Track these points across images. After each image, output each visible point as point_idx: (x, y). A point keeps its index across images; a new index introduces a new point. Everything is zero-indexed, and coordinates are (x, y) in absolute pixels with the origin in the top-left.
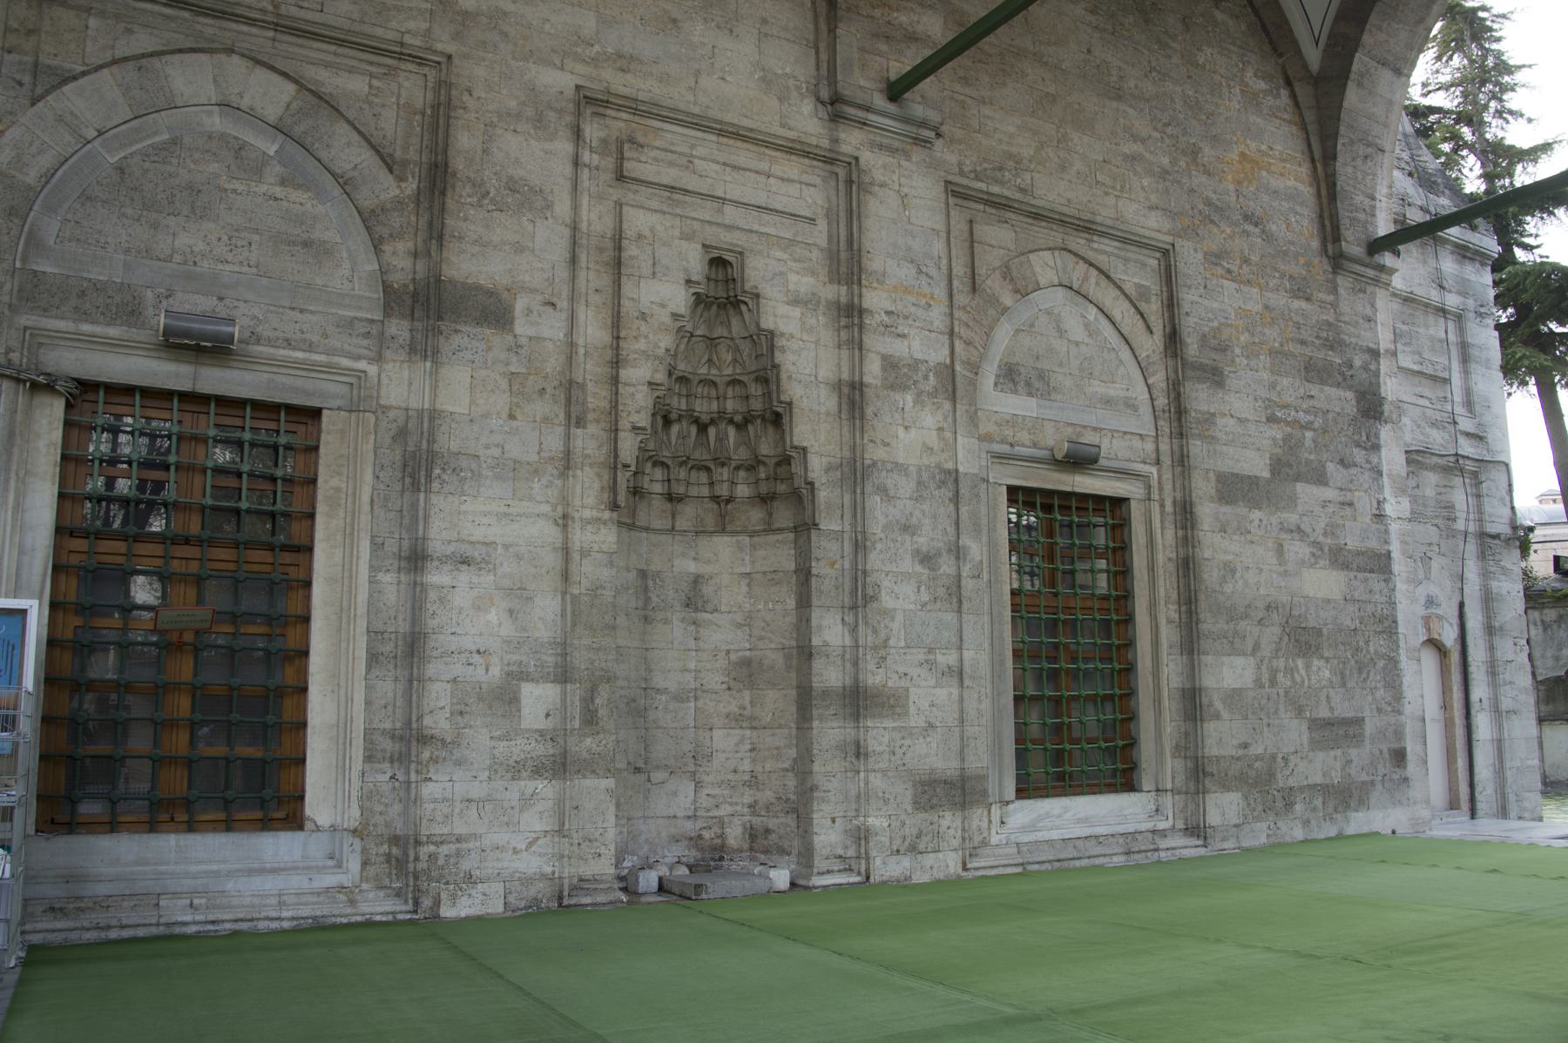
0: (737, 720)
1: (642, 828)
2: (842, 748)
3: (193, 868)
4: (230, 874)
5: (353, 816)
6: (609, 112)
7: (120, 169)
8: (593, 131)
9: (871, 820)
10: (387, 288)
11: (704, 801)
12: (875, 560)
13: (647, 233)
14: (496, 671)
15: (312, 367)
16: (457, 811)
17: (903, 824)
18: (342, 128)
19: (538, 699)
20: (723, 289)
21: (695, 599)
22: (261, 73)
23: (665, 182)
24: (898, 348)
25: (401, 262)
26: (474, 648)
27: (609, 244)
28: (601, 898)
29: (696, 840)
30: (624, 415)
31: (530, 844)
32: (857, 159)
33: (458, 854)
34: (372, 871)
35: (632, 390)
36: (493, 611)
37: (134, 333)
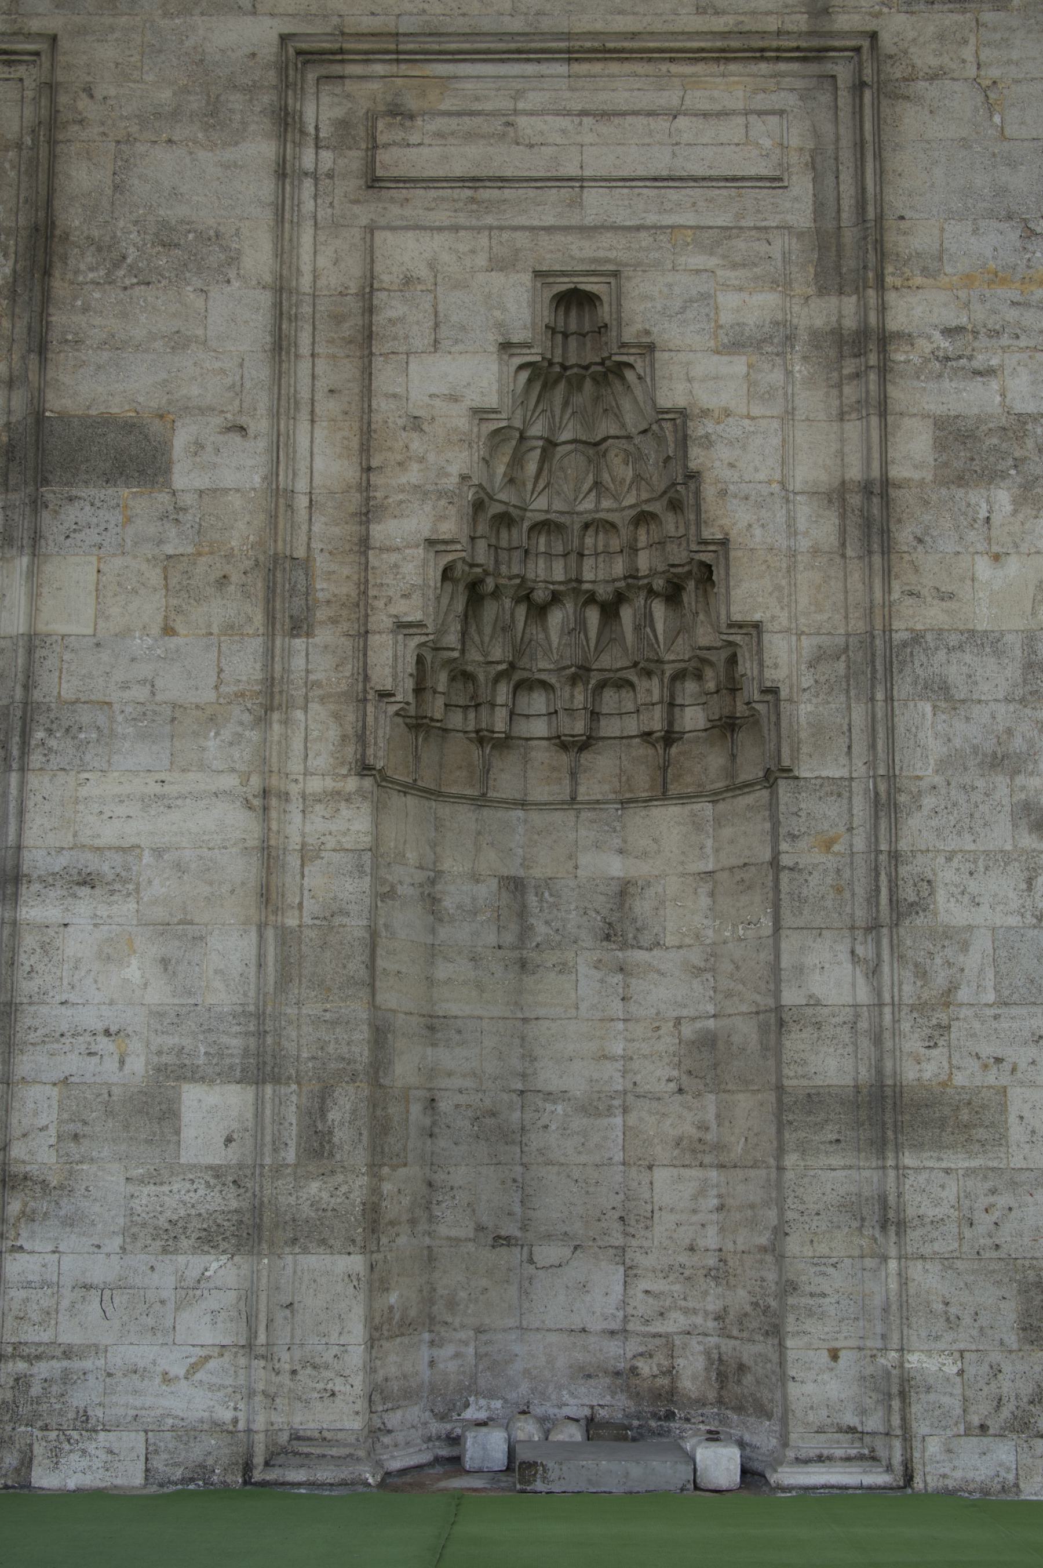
0: (697, 1150)
1: (517, 1348)
2: (852, 1208)
8: (320, 110)
9: (914, 1360)
11: (641, 1306)
12: (917, 830)
13: (423, 272)
14: (137, 1065)
16: (65, 1303)
17: (996, 1371)
19: (212, 1115)
20: (582, 349)
21: (619, 925)
23: (458, 171)
24: (974, 399)
26: (100, 1026)
27: (353, 305)
28: (325, 1474)
29: (624, 1377)
30: (380, 604)
31: (194, 1368)
32: (874, 36)
33: (66, 1377)
35: (394, 558)
36: (134, 962)
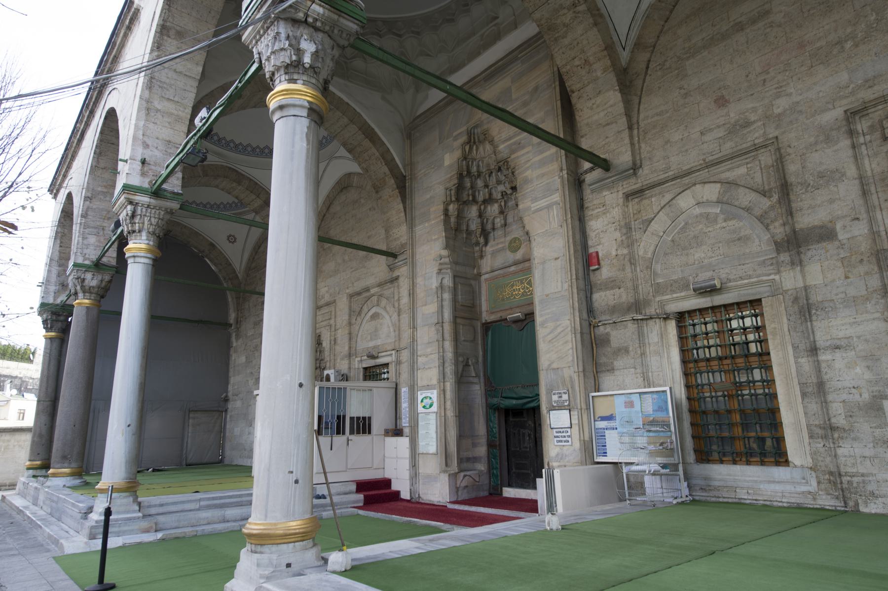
3: (748, 479)
4: (761, 482)
5: (809, 462)
6: (870, 111)
7: (673, 241)
10: (776, 243)
15: (752, 284)
18: (741, 190)
22: (707, 186)
25: (779, 230)
26: (851, 386)
33: (864, 482)
34: (823, 486)
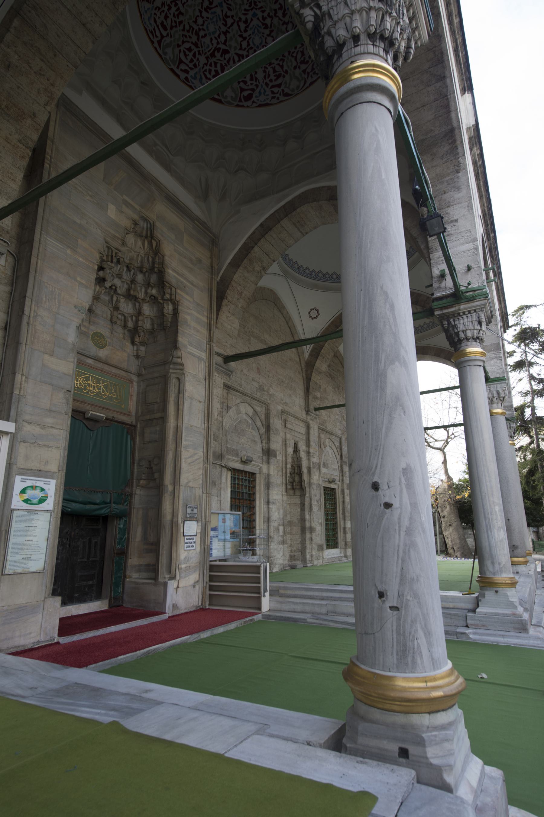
20: (296, 450)
37: (236, 459)
